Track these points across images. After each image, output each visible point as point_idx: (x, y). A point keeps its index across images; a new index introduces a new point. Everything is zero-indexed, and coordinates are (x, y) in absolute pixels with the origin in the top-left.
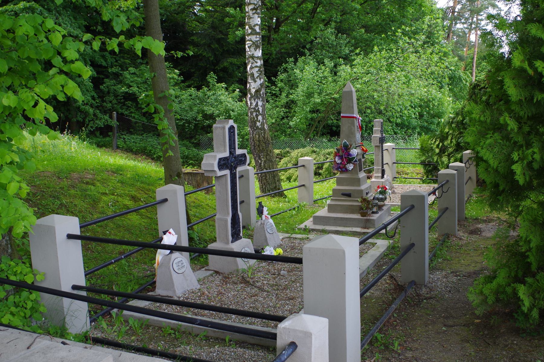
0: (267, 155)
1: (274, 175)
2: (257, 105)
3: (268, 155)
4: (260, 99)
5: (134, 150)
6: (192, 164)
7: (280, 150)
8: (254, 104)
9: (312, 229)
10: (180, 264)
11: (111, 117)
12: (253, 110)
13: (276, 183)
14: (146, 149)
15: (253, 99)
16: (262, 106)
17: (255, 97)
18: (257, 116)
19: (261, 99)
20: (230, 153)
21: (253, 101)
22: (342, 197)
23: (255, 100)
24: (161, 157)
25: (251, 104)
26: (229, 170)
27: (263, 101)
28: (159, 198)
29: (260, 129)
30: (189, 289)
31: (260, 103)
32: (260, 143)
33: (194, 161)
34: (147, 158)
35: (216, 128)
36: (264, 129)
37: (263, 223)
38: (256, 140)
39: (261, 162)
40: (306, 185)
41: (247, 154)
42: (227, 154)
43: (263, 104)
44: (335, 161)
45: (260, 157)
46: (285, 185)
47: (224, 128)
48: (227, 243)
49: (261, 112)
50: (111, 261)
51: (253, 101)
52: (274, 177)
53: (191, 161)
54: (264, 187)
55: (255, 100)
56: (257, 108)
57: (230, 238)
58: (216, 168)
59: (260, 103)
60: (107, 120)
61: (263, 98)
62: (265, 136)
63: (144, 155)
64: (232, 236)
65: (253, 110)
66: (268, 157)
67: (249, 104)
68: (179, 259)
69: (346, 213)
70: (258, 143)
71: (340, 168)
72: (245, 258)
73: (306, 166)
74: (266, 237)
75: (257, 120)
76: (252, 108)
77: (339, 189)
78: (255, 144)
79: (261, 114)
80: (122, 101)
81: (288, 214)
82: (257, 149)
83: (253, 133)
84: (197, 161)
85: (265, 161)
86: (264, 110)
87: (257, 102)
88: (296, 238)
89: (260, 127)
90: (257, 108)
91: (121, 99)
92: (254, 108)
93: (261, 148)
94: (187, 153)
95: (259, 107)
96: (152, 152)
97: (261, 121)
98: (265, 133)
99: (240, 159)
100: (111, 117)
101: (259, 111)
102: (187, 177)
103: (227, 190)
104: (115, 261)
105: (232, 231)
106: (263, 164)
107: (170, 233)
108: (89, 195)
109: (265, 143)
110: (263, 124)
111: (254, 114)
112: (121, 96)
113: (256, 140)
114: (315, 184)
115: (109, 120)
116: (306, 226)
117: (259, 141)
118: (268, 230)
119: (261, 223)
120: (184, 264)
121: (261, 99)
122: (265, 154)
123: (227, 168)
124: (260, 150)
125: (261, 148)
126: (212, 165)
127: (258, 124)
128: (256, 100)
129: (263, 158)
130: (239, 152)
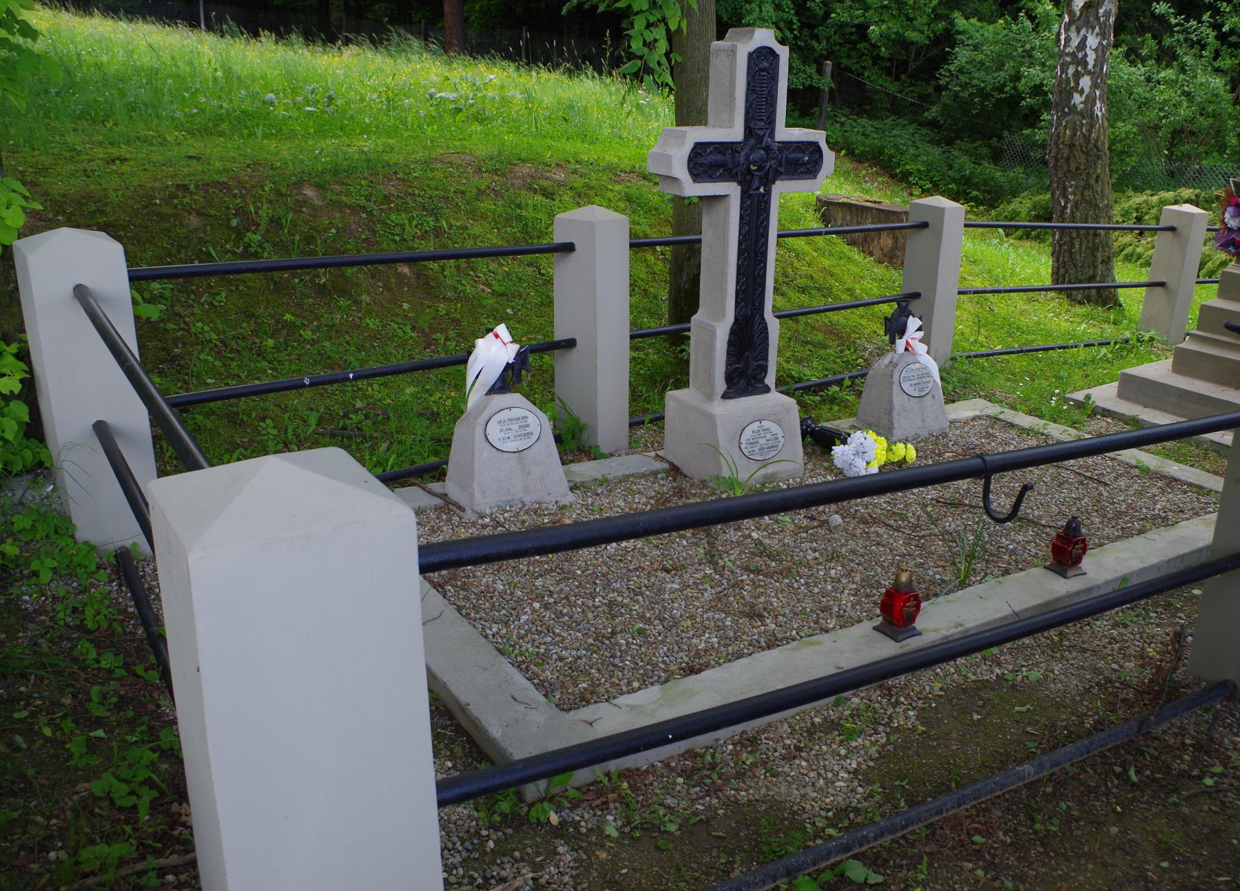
0: (1084, 188)
1: (1094, 243)
2: (1082, 45)
3: (1088, 186)
4: (1093, 29)
5: (857, 151)
6: (975, 199)
7: (1197, 191)
8: (1075, 41)
9: (1104, 409)
10: (515, 427)
11: (820, 71)
12: (1068, 59)
13: (1095, 267)
14: (881, 153)
15: (1073, 28)
16: (1096, 50)
17: (1080, 23)
18: (1077, 76)
19: (1097, 29)
20: (749, 130)
21: (1073, 35)
22: (1222, 334)
23: (1078, 31)
24: (911, 174)
25: (1068, 40)
26: (740, 183)
27: (1103, 35)
28: (559, 238)
29: (1081, 114)
30: (527, 500)
31: (1092, 41)
32: (1072, 151)
33: (983, 192)
34: (882, 172)
35: (718, 51)
36: (1091, 115)
37: (894, 360)
38: (1063, 143)
39: (1066, 203)
40: (1170, 284)
41: (824, 146)
42: (734, 132)
43: (1100, 43)
44: (1223, 221)
45: (1065, 189)
46: (1123, 273)
47: (733, 52)
48: (710, 397)
49: (1090, 67)
50: (297, 377)
51: (1073, 35)
52: (1094, 249)
53: (975, 193)
54: (1062, 271)
55: (1078, 31)
56: (1080, 55)
57: (720, 385)
58: (680, 170)
59: (1092, 41)
60: (811, 77)
61: (1103, 27)
62: (1090, 132)
63: (876, 165)
64: (729, 378)
65: (1068, 59)
66: (1086, 193)
67: (1063, 42)
68: (516, 413)
69: (1223, 384)
70: (1066, 152)
71: (1234, 245)
72: (1148, 444)
73: (1179, 229)
74: (891, 403)
75: (1076, 89)
76: (1068, 54)
77: (1221, 310)
78: (1058, 153)
79: (1089, 73)
80: (854, 37)
81: (1082, 354)
82: (1062, 167)
83: (1059, 124)
84: (989, 192)
85: (1076, 205)
86: (1099, 62)
87: (1085, 39)
88: (1012, 426)
89: (1080, 107)
90: (1080, 55)
91: (851, 34)
92: (1073, 55)
93: (1073, 167)
94: (968, 172)
95: (1088, 51)
96: (894, 160)
97: (1087, 90)
98: (1092, 126)
99: (792, 155)
100: (820, 71)
101: (1086, 64)
102: (840, 215)
103: (725, 244)
104: (311, 385)
105: (729, 364)
106: (1069, 211)
107: (497, 336)
108: (519, 218)
109: (1087, 154)
110: (1090, 101)
111: (1071, 70)
112: (852, 27)
113: (1063, 143)
114: (1198, 287)
115: (816, 77)
116: (1088, 397)
117: (1072, 146)
118: (905, 386)
119: (891, 362)
120: (529, 430)
121: (1097, 29)
122: (1082, 184)
123: (728, 176)
124: (1069, 171)
125: (1073, 167)
126: (668, 159)
127: (1077, 99)
128: (1083, 31)
129: (1074, 194)
130: (785, 133)
